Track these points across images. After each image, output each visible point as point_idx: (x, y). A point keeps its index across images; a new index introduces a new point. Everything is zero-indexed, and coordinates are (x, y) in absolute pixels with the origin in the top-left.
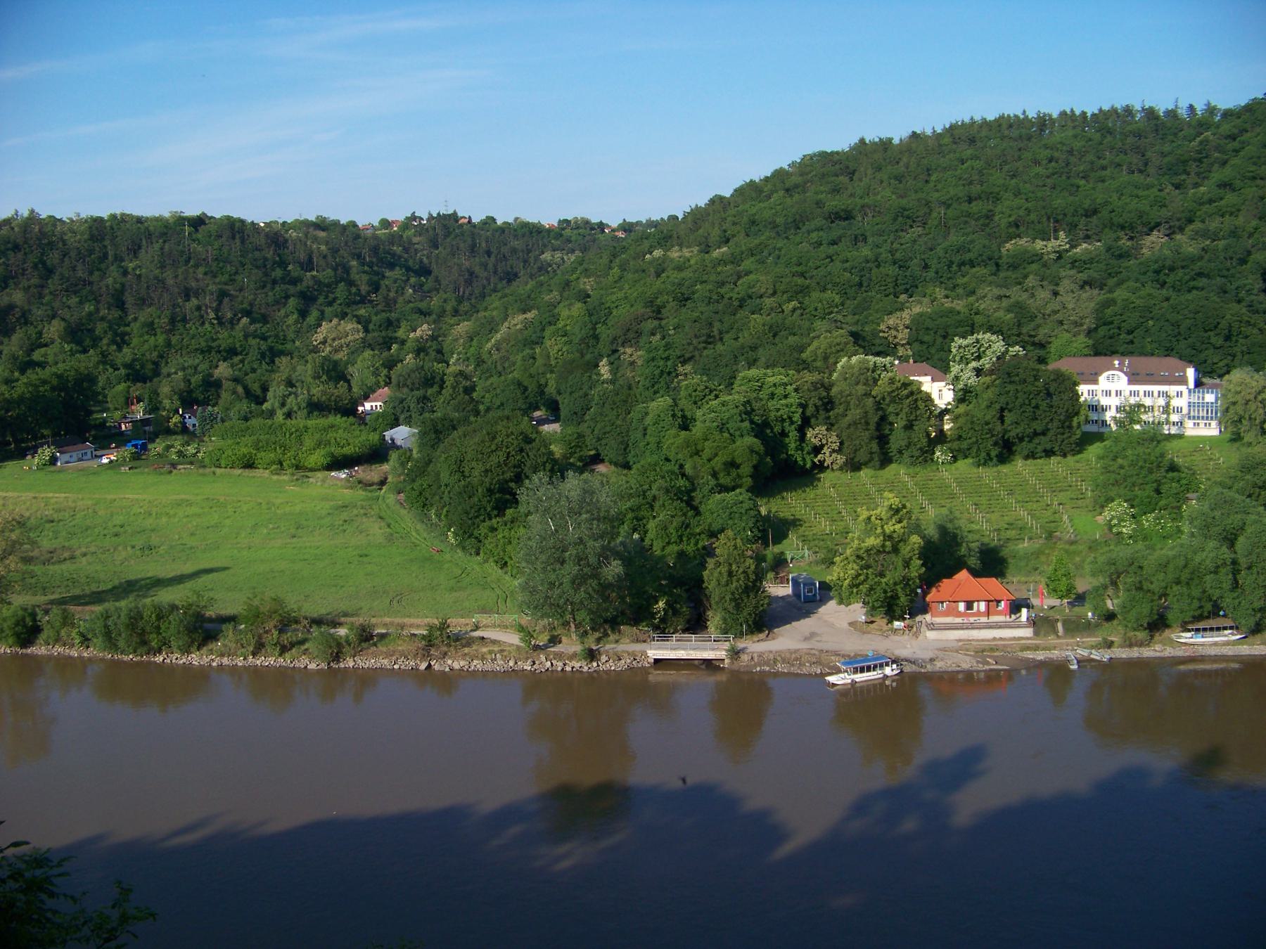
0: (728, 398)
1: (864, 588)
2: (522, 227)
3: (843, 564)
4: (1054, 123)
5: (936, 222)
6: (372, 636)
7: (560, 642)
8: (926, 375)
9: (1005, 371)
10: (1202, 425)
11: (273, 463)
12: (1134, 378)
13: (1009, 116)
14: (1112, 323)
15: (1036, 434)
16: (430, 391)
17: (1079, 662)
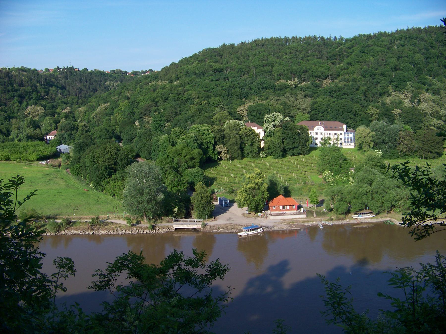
0: (188, 135)
1: (249, 202)
2: (98, 73)
3: (240, 193)
4: (290, 40)
5: (252, 74)
6: (70, 223)
7: (140, 223)
8: (255, 127)
9: (284, 126)
10: (348, 144)
11: (17, 158)
12: (326, 128)
13: (275, 37)
14: (316, 109)
15: (294, 148)
16: (73, 132)
17: (323, 226)
